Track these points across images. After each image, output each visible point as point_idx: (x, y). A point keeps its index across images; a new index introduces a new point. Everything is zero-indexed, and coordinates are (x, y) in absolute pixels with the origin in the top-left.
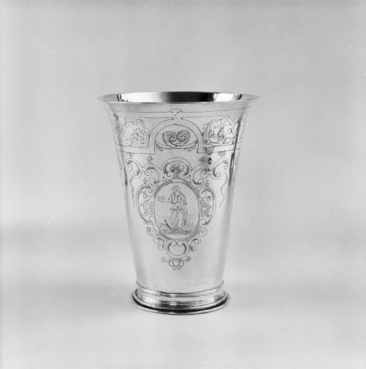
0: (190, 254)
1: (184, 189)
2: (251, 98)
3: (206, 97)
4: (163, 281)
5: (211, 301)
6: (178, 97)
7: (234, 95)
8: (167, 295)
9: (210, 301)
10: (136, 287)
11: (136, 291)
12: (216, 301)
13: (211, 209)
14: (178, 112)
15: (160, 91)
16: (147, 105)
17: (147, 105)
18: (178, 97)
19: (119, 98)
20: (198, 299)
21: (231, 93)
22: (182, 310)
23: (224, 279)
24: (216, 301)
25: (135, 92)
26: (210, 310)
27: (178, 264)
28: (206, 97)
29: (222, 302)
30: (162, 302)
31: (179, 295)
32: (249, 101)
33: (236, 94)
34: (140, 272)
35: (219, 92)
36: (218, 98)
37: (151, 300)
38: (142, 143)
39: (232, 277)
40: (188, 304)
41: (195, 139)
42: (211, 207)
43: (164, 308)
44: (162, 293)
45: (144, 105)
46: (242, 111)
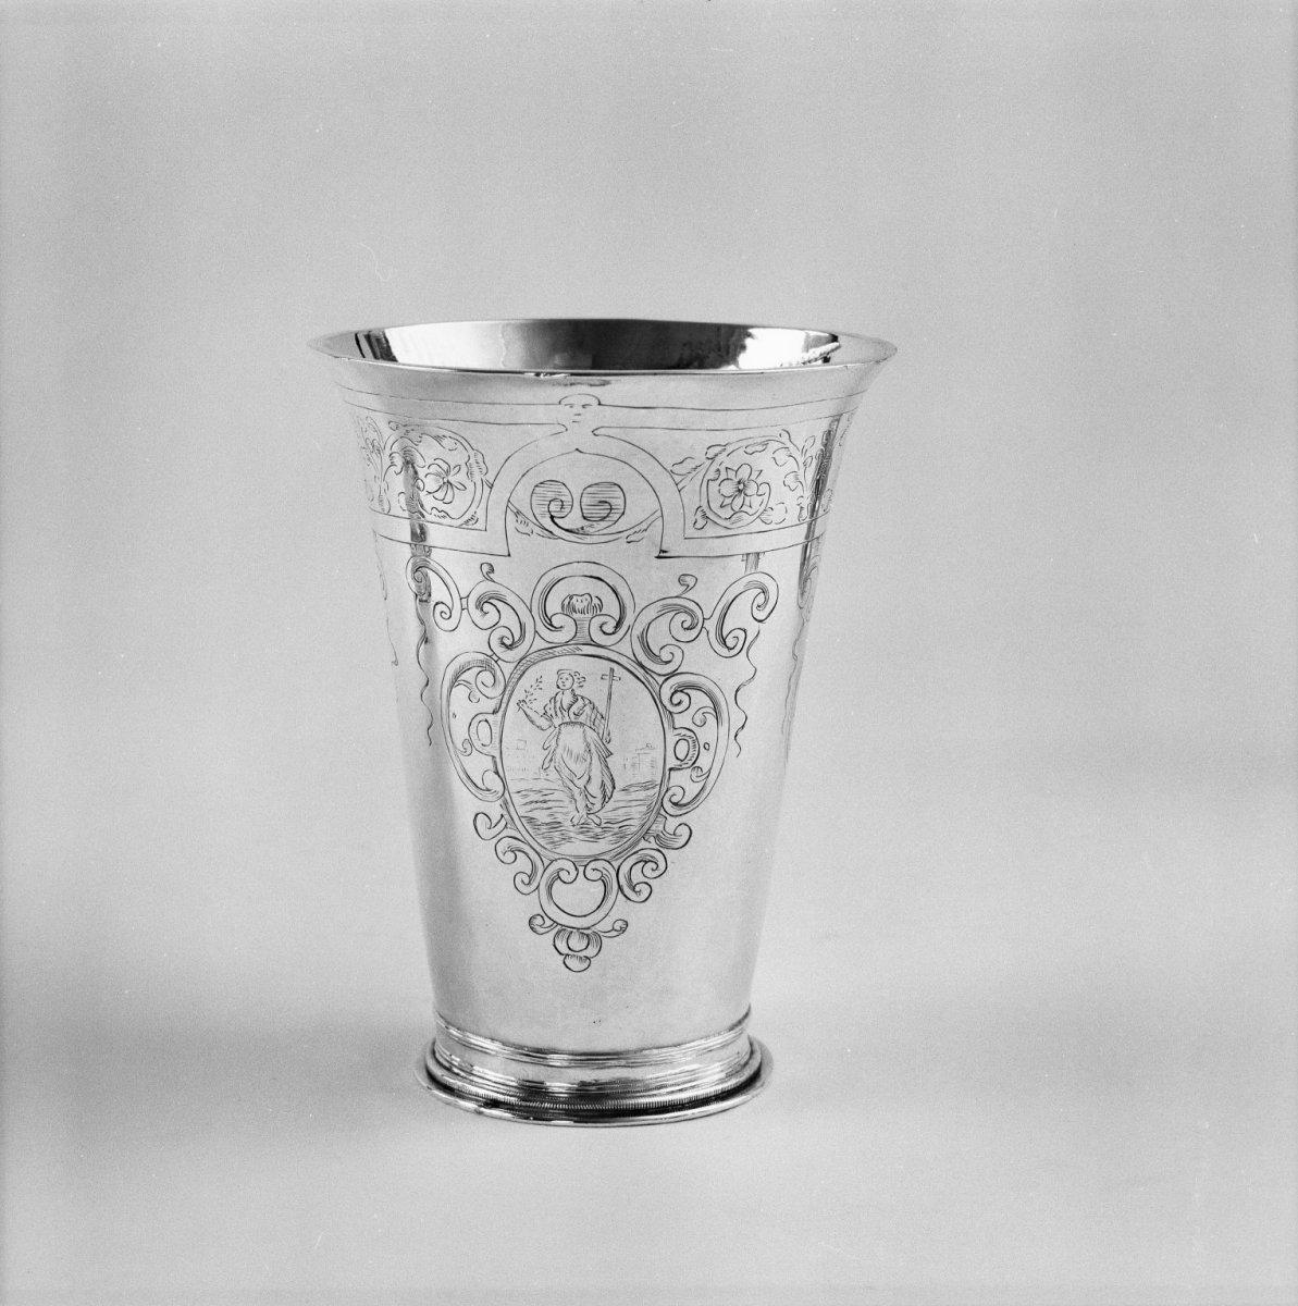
0: (621, 908)
2: (882, 353)
3: (703, 347)
6: (595, 346)
7: (808, 336)
8: (538, 1054)
12: (729, 1076)
14: (584, 406)
16: (482, 379)
17: (501, 378)
18: (595, 346)
19: (380, 348)
21: (764, 327)
22: (598, 1105)
24: (729, 1076)
25: (427, 322)
27: (581, 942)
28: (703, 347)
33: (812, 334)
35: (757, 323)
36: (758, 354)
37: (496, 1074)
39: (784, 996)
41: (653, 505)
42: (707, 746)
43: (532, 1103)
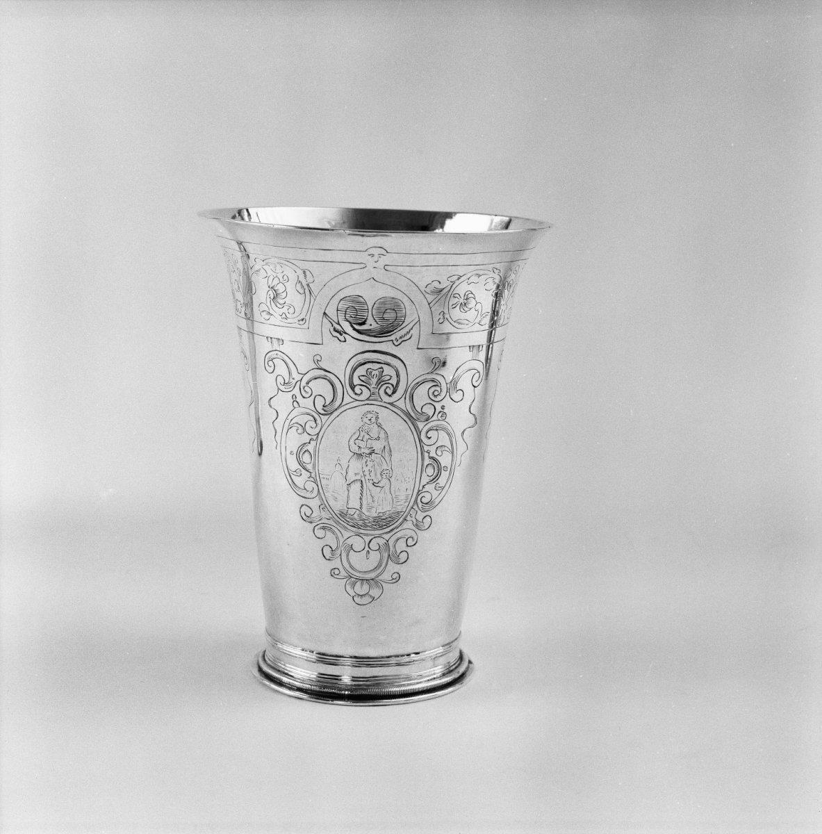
1: (394, 424)
3: (424, 222)
4: (325, 627)
5: (431, 673)
9: (434, 674)
10: (263, 642)
11: (265, 651)
12: (444, 675)
13: (444, 475)
15: (341, 206)
17: (311, 233)
18: (369, 221)
20: (403, 671)
22: (364, 695)
23: (463, 628)
24: (444, 675)
26: (431, 694)
29: (456, 677)
30: (354, 681)
31: (361, 661)
32: (532, 233)
34: (275, 611)
37: (305, 673)
38: (304, 321)
40: (388, 679)
43: (325, 692)
44: (323, 658)
45: (325, 233)
46: (508, 257)
